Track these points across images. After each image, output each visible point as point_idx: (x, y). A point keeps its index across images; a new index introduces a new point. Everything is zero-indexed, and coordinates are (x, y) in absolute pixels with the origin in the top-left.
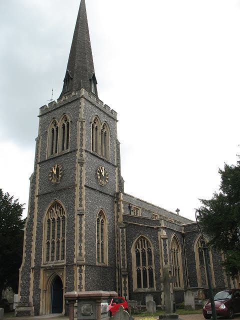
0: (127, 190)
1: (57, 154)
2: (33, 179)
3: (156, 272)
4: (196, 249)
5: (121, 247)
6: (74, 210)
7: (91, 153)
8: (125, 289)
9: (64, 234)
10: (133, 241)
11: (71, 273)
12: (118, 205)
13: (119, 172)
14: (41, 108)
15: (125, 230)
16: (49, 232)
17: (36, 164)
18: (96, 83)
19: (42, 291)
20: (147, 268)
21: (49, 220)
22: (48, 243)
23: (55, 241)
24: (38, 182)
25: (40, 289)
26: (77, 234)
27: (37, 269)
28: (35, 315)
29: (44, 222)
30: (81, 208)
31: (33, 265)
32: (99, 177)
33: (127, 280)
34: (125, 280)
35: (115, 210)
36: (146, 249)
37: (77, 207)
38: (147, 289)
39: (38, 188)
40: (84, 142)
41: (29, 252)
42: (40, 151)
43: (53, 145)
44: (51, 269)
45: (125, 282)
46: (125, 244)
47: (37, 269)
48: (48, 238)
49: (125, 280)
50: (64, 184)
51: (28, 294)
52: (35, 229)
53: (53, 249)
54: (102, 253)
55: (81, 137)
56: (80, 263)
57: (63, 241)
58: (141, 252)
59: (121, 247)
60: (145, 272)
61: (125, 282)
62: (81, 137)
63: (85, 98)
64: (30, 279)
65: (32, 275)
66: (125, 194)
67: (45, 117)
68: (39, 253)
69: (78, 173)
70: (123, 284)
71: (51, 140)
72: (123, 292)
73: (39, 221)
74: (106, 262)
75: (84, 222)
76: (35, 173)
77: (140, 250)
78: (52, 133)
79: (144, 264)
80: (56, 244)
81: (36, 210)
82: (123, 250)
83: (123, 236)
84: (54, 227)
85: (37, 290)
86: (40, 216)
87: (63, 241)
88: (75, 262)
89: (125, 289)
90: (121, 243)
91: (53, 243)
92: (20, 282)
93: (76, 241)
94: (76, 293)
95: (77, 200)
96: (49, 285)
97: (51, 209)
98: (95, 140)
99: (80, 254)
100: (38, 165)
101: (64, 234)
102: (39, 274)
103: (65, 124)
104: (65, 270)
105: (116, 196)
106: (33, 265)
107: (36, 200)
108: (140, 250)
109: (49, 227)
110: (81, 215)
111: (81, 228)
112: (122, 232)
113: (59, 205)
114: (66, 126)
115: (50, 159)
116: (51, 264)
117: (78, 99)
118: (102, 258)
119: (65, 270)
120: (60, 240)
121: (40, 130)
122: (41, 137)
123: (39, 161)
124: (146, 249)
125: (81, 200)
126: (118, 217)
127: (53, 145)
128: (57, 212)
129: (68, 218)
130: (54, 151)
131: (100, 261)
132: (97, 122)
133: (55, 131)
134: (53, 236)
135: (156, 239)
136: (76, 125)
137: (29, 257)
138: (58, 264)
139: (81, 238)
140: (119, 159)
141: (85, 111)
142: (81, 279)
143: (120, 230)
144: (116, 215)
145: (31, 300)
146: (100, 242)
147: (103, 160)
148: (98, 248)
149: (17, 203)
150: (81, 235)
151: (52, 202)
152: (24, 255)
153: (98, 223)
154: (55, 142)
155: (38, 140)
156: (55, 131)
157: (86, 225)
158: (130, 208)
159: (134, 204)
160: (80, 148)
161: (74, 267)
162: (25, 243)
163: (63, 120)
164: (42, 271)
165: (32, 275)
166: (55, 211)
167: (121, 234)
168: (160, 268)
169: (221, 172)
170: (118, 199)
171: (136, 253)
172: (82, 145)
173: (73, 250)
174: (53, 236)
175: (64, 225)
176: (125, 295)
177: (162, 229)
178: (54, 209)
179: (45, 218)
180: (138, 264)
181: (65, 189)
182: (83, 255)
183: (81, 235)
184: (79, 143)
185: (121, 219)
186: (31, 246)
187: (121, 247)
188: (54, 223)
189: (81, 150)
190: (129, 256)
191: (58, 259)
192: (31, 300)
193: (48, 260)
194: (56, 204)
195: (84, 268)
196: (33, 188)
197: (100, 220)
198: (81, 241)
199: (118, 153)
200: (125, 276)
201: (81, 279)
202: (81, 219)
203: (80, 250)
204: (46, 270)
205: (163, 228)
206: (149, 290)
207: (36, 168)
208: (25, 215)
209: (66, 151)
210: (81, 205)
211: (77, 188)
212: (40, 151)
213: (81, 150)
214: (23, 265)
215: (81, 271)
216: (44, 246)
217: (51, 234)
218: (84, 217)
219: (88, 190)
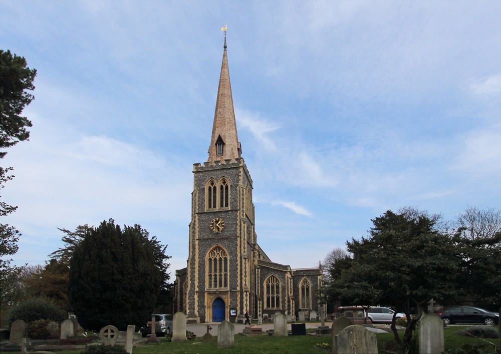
1: (229, 208)
2: (192, 226)
4: (300, 286)
12: (254, 253)
13: (254, 229)
15: (259, 270)
19: (206, 307)
20: (271, 296)
21: (210, 259)
22: (210, 276)
28: (201, 323)
29: (206, 260)
36: (275, 284)
38: (275, 308)
44: (215, 293)
45: (260, 304)
50: (227, 234)
51: (194, 309)
53: (215, 279)
60: (273, 298)
61: (260, 304)
64: (194, 299)
67: (201, 174)
77: (270, 284)
79: (273, 293)
81: (197, 251)
86: (202, 256)
88: (206, 290)
100: (196, 215)
102: (204, 296)
107: (197, 242)
108: (270, 284)
112: (258, 271)
116: (213, 289)
122: (198, 192)
123: (197, 212)
124: (275, 284)
137: (193, 284)
144: (252, 259)
149: (154, 240)
161: (238, 293)
164: (206, 294)
169: (348, 244)
171: (267, 286)
178: (215, 252)
180: (268, 293)
181: (227, 238)
186: (194, 276)
190: (262, 287)
192: (196, 313)
200: (260, 300)
202: (245, 261)
203: (246, 282)
204: (209, 293)
206: (277, 309)
209: (225, 208)
210: (244, 252)
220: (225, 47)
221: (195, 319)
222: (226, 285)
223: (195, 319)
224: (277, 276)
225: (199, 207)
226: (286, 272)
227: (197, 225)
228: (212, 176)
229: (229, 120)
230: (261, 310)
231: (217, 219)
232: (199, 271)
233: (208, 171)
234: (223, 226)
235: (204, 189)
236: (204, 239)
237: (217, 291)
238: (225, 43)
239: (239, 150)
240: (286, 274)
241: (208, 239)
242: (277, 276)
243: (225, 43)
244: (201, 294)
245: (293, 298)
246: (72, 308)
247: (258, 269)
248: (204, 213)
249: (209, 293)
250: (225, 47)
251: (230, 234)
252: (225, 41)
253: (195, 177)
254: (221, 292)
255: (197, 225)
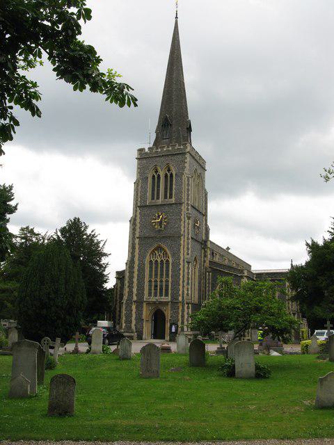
2: (133, 222)
12: (205, 252)
13: (206, 220)
16: (151, 271)
22: (150, 281)
24: (138, 225)
27: (140, 303)
30: (188, 256)
31: (135, 298)
35: (203, 256)
39: (138, 230)
42: (139, 194)
44: (154, 303)
47: (140, 303)
51: (131, 322)
65: (134, 307)
66: (211, 242)
68: (140, 288)
85: (139, 319)
96: (150, 316)
104: (169, 306)
105: (203, 242)
107: (137, 241)
112: (209, 276)
116: (153, 299)
117: (185, 153)
119: (169, 306)
123: (139, 205)
126: (205, 261)
133: (156, 179)
137: (131, 292)
140: (206, 209)
149: (93, 233)
151: (156, 245)
156: (156, 179)
159: (216, 250)
164: (145, 305)
165: (134, 307)
168: (179, 295)
170: (206, 245)
172: (188, 199)
174: (156, 275)
181: (170, 237)
185: (207, 264)
192: (133, 327)
194: (159, 248)
196: (133, 230)
204: (149, 303)
207: (135, 211)
209: (169, 201)
216: (146, 284)
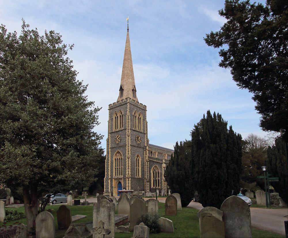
0: (150, 143)
3: (160, 181)
5: (147, 170)
6: (126, 155)
7: (133, 130)
8: (148, 187)
9: (122, 165)
10: (152, 167)
11: (125, 181)
12: (146, 152)
13: (147, 136)
14: (109, 105)
15: (148, 163)
16: (116, 164)
17: (109, 134)
18: (136, 91)
19: (114, 187)
20: (157, 179)
21: (116, 159)
22: (116, 169)
23: (119, 168)
24: (110, 142)
25: (113, 187)
26: (127, 165)
29: (113, 160)
30: (128, 155)
31: (110, 177)
32: (137, 140)
33: (149, 183)
34: (148, 183)
35: (145, 154)
36: (157, 171)
37: (127, 154)
39: (110, 145)
40: (129, 126)
41: (108, 172)
42: (110, 127)
43: (116, 124)
44: (117, 179)
46: (148, 169)
48: (116, 166)
49: (148, 183)
50: (122, 144)
51: (108, 188)
52: (110, 162)
54: (138, 173)
55: (128, 123)
56: (128, 177)
57: (122, 168)
58: (157, 172)
59: (146, 169)
61: (148, 184)
62: (128, 123)
63: (130, 103)
65: (109, 181)
68: (112, 172)
69: (127, 139)
70: (147, 185)
71: (115, 123)
72: (147, 188)
73: (112, 159)
74: (140, 176)
75: (130, 161)
76: (109, 138)
78: (115, 119)
80: (119, 169)
81: (110, 154)
82: (148, 171)
83: (147, 165)
84: (118, 162)
85: (112, 187)
86: (112, 157)
87: (122, 168)
88: (127, 176)
89: (148, 187)
90: (147, 168)
91: (118, 168)
92: (105, 184)
93: (127, 168)
94: (10, 121)
95: (127, 151)
97: (116, 154)
98: (135, 123)
99: (128, 174)
100: (110, 134)
101: (122, 165)
102: (112, 181)
103: (121, 115)
104: (123, 180)
106: (110, 177)
109: (116, 162)
110: (128, 158)
111: (129, 163)
112: (147, 164)
113: (119, 153)
114: (121, 116)
115: (115, 132)
117: (126, 104)
118: (138, 175)
119: (123, 180)
120: (121, 167)
121: (109, 116)
123: (110, 132)
124: (157, 171)
125: (128, 151)
127: (116, 124)
128: (119, 156)
129: (124, 159)
130: (117, 128)
131: (138, 176)
132: (136, 114)
133: (117, 118)
134: (118, 165)
135: (161, 167)
136: (126, 117)
137: (108, 174)
138: (120, 177)
139: (129, 167)
141: (129, 109)
142: (129, 183)
143: (147, 163)
144: (145, 156)
145: (109, 191)
146: (138, 168)
147: (139, 132)
148: (137, 171)
149: (101, 148)
150: (129, 166)
151: (117, 151)
152: (106, 173)
153: (137, 160)
154: (117, 123)
155: (109, 122)
157: (131, 162)
158: (152, 152)
160: (127, 128)
162: (106, 168)
163: (120, 113)
164: (113, 179)
166: (118, 155)
167: (147, 165)
172: (128, 127)
173: (126, 172)
174: (118, 165)
175: (122, 161)
176: (148, 189)
177: (163, 163)
179: (114, 157)
181: (122, 146)
182: (130, 174)
183: (129, 166)
184: (127, 126)
185: (147, 158)
186: (109, 169)
187: (146, 169)
188: (118, 160)
189: (128, 129)
190: (150, 174)
191: (120, 175)
192: (109, 191)
193: (116, 175)
194: (118, 152)
195: (130, 179)
197: (138, 159)
198: (128, 169)
199: (147, 127)
200: (148, 182)
201: (129, 183)
202: (128, 159)
204: (115, 179)
205: (164, 163)
208: (105, 154)
210: (128, 154)
211: (127, 146)
212: (110, 127)
213: (128, 129)
214: (105, 177)
215: (129, 180)
216: (114, 170)
217: (119, 174)
218: (130, 159)
219: (132, 147)
220: (128, 30)
221: (109, 194)
222: (122, 175)
223: (109, 194)
224: (157, 166)
225: (111, 129)
226: (162, 163)
227: (110, 140)
228: (116, 111)
229: (127, 74)
230: (149, 188)
231: (118, 136)
232: (111, 167)
233: (114, 108)
234: (120, 139)
235: (113, 118)
236: (113, 148)
237: (118, 178)
238: (128, 27)
239: (101, 108)
240: (162, 165)
241: (114, 148)
242: (157, 166)
243: (128, 27)
244: (111, 179)
245: (165, 180)
246: (138, 187)
247: (148, 162)
248: (113, 132)
249: (115, 179)
250: (128, 30)
251: (123, 143)
252: (128, 26)
253: (109, 112)
254: (119, 179)
255: (110, 140)
